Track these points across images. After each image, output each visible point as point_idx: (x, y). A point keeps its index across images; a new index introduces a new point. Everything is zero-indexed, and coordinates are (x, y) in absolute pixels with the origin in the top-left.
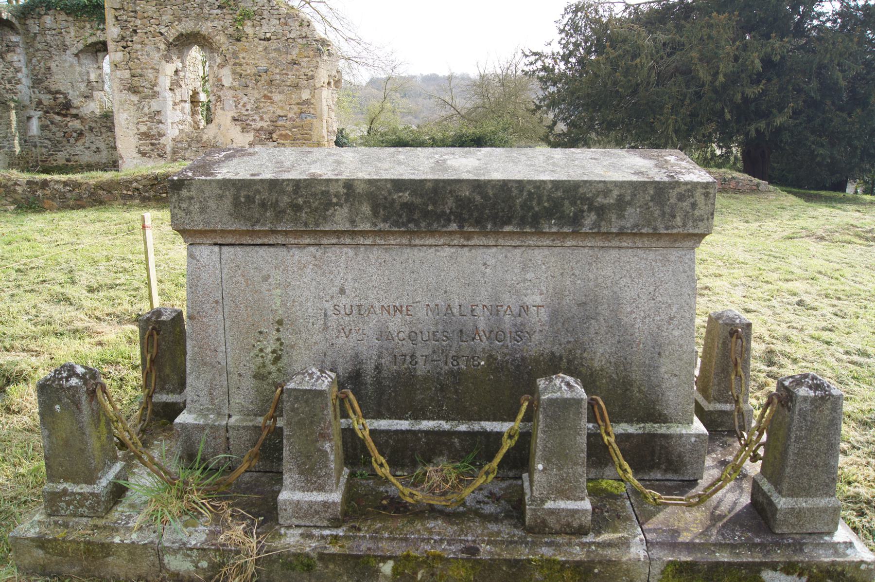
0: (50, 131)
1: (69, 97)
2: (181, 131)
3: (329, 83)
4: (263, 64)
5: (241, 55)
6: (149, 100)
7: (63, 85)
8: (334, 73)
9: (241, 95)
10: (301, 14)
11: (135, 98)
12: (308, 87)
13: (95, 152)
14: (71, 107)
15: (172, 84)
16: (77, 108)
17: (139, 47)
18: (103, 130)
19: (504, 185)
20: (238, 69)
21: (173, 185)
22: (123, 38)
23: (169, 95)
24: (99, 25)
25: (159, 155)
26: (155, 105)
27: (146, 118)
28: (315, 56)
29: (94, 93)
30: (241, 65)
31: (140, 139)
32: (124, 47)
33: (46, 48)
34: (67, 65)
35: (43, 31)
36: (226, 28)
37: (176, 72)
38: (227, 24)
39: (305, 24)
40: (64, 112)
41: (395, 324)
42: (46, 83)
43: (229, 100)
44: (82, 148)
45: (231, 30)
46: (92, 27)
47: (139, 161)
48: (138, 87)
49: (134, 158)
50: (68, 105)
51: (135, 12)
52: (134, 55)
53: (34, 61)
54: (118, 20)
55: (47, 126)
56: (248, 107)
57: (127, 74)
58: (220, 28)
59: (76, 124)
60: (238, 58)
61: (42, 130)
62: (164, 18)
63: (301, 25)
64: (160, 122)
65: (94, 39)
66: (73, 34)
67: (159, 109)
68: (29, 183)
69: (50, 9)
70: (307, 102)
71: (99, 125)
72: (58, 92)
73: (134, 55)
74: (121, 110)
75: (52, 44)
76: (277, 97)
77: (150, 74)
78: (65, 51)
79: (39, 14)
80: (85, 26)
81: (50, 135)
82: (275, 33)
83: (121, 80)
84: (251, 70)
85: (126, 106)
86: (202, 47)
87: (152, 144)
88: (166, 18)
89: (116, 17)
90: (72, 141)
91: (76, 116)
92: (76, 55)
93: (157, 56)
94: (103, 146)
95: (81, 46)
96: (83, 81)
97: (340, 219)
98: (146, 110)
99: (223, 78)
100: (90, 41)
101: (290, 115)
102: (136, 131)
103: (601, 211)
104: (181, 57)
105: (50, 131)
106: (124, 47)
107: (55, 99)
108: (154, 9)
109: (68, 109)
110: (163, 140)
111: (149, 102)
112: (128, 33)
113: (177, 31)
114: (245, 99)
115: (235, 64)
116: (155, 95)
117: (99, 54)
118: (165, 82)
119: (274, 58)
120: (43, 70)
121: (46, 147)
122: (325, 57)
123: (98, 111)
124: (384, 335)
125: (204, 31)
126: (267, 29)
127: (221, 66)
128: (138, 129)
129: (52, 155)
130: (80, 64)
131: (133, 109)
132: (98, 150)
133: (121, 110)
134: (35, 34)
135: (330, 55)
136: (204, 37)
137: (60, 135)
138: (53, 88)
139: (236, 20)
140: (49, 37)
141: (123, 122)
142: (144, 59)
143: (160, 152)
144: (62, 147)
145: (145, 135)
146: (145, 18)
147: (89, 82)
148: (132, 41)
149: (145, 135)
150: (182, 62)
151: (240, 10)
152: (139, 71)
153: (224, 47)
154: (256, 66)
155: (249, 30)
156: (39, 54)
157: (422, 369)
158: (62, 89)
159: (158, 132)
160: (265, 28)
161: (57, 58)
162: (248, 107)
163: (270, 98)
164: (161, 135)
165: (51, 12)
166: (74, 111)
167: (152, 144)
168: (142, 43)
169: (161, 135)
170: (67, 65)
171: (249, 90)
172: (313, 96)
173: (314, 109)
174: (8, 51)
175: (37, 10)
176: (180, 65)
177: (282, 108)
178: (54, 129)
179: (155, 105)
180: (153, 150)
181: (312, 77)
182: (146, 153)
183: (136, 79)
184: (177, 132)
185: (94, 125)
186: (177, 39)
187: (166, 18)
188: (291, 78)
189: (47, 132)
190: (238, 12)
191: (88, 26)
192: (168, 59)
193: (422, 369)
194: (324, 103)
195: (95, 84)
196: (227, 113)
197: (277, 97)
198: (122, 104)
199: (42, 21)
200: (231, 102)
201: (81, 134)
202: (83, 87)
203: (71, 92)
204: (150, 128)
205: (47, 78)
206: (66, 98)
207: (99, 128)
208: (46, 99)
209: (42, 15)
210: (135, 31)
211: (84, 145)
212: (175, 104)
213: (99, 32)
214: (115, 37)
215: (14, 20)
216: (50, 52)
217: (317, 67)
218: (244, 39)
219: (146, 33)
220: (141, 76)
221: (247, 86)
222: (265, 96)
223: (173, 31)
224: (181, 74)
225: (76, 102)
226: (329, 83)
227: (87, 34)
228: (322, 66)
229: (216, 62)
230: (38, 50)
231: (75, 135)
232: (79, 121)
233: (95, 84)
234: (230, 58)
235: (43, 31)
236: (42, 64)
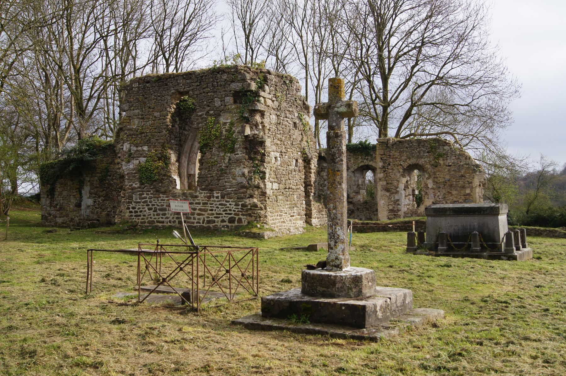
2: (408, 209)
3: (480, 185)
4: (448, 177)
5: (437, 174)
8: (482, 180)
9: (437, 191)
10: (466, 154)
11: (388, 194)
12: (469, 187)
15: (405, 187)
18: (364, 210)
19: (470, 208)
20: (436, 180)
22: (384, 167)
23: (403, 192)
26: (397, 197)
27: (392, 203)
28: (472, 173)
30: (437, 178)
36: (431, 161)
37: (407, 182)
38: (431, 160)
39: (468, 158)
41: (456, 228)
45: (433, 162)
46: (362, 158)
51: (390, 155)
52: (388, 175)
56: (440, 197)
57: (385, 183)
60: (435, 175)
63: (466, 159)
64: (399, 204)
65: (362, 164)
66: (352, 161)
68: (362, 224)
70: (469, 194)
73: (388, 175)
76: (454, 192)
77: (395, 183)
82: (453, 163)
84: (441, 180)
85: (384, 197)
86: (419, 170)
87: (395, 215)
89: (381, 158)
92: (353, 172)
93: (398, 175)
95: (356, 167)
96: (355, 185)
97: (448, 213)
98: (393, 199)
100: (360, 165)
101: (460, 201)
103: (484, 211)
104: (409, 175)
110: (399, 213)
114: (439, 193)
115: (434, 178)
116: (397, 192)
118: (402, 186)
119: (453, 174)
122: (478, 173)
123: (361, 200)
124: (454, 229)
125: (420, 163)
126: (450, 161)
127: (428, 179)
130: (355, 176)
131: (386, 198)
135: (480, 172)
136: (420, 166)
139: (435, 158)
141: (382, 205)
142: (393, 176)
145: (391, 211)
147: (358, 185)
149: (391, 211)
150: (410, 177)
154: (444, 178)
155: (441, 162)
157: (460, 234)
160: (449, 161)
162: (440, 197)
163: (451, 193)
164: (399, 210)
167: (395, 215)
168: (392, 169)
169: (399, 210)
171: (441, 189)
172: (472, 192)
173: (472, 198)
174: (322, 171)
176: (409, 178)
177: (456, 197)
179: (397, 197)
181: (471, 183)
184: (406, 209)
185: (359, 207)
186: (408, 167)
188: (461, 183)
191: (360, 157)
192: (403, 176)
193: (460, 234)
194: (477, 195)
195: (361, 186)
197: (454, 192)
198: (382, 196)
202: (355, 188)
204: (394, 207)
210: (389, 164)
212: (406, 196)
215: (326, 156)
217: (473, 178)
220: (391, 184)
221: (440, 188)
222: (449, 192)
224: (409, 182)
226: (480, 185)
228: (476, 177)
233: (361, 186)
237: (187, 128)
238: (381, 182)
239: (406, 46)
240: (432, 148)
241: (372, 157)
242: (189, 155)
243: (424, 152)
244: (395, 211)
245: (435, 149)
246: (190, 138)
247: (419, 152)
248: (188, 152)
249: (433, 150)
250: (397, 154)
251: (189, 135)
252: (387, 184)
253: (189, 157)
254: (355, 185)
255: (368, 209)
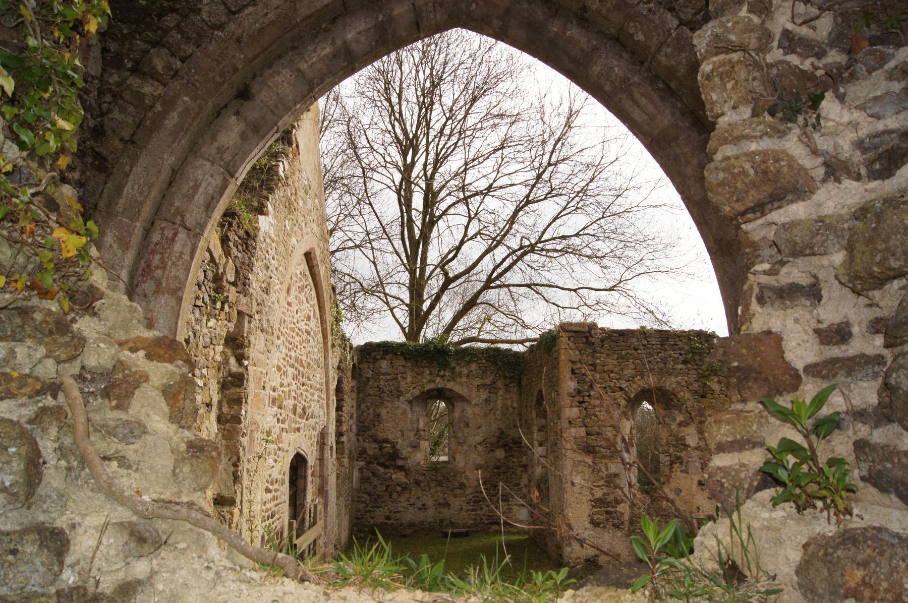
0: (371, 483)
1: (397, 447)
6: (607, 461)
7: (392, 433)
11: (589, 460)
13: (420, 509)
14: (398, 457)
16: (405, 459)
17: (597, 402)
18: (432, 484)
21: (362, 540)
22: (579, 392)
24: (439, 371)
25: (614, 525)
27: (602, 482)
29: (422, 442)
31: (593, 507)
32: (580, 403)
33: (378, 393)
34: (399, 412)
35: (377, 375)
36: (691, 384)
40: (388, 463)
42: (373, 431)
43: (695, 462)
44: (405, 504)
45: (695, 386)
46: (431, 374)
47: (591, 532)
48: (594, 447)
49: (586, 529)
50: (395, 455)
53: (363, 406)
54: (575, 374)
55: (369, 478)
57: (582, 432)
58: (684, 384)
59: (400, 476)
60: (703, 415)
61: (361, 483)
62: (626, 372)
66: (409, 379)
67: (617, 472)
69: (387, 354)
71: (428, 478)
72: (386, 441)
74: (575, 473)
75: (385, 389)
78: (398, 397)
79: (375, 358)
80: (423, 372)
81: (370, 489)
83: (575, 438)
85: (580, 469)
87: (608, 513)
88: (628, 372)
90: (395, 495)
91: (401, 468)
92: (410, 402)
93: (616, 413)
94: (430, 502)
95: (417, 393)
96: (413, 430)
99: (687, 437)
102: (590, 497)
105: (371, 483)
106: (580, 403)
107: (381, 448)
108: (615, 362)
109: (394, 460)
111: (606, 464)
112: (586, 387)
113: (639, 386)
117: (429, 401)
120: (371, 417)
121: (363, 502)
123: (422, 462)
128: (593, 495)
129: (370, 511)
131: (588, 471)
132: (424, 507)
133: (575, 473)
134: (368, 378)
137: (381, 488)
138: (381, 436)
140: (382, 382)
142: (602, 415)
143: (616, 521)
144: (383, 502)
145: (598, 502)
146: (604, 371)
147: (418, 430)
148: (589, 396)
149: (598, 502)
151: (706, 365)
152: (596, 428)
153: (689, 404)
156: (369, 399)
158: (391, 437)
159: (615, 498)
161: (389, 404)
165: (388, 357)
166: (400, 463)
167: (608, 513)
170: (399, 412)
175: (373, 354)
178: (375, 481)
180: (608, 520)
182: (600, 523)
183: (593, 437)
185: (420, 478)
187: (628, 372)
189: (367, 485)
190: (704, 367)
195: (422, 433)
196: (693, 476)
199: (377, 365)
200: (697, 464)
201: (405, 488)
203: (400, 441)
205: (374, 425)
206: (393, 447)
207: (428, 482)
208: (372, 448)
209: (378, 360)
211: (408, 500)
213: (439, 378)
214: (572, 391)
216: (382, 398)
218: (709, 396)
219: (605, 388)
220: (598, 434)
223: (634, 386)
225: (404, 453)
227: (425, 381)
229: (674, 420)
230: (369, 395)
231: (399, 489)
232: (403, 473)
233: (422, 433)
234: (696, 416)
235: (377, 375)
236: (371, 411)
237: (159, 64)
238: (573, 430)
239: (449, 194)
240: (694, 353)
241: (453, 373)
242: (147, 233)
243: (675, 361)
244: (608, 504)
245: (700, 354)
246: (173, 118)
247: (664, 361)
248: (147, 210)
249: (697, 357)
250: (612, 363)
251: (169, 105)
252: (588, 434)
253: (145, 248)
254: (413, 430)
255: (440, 484)
